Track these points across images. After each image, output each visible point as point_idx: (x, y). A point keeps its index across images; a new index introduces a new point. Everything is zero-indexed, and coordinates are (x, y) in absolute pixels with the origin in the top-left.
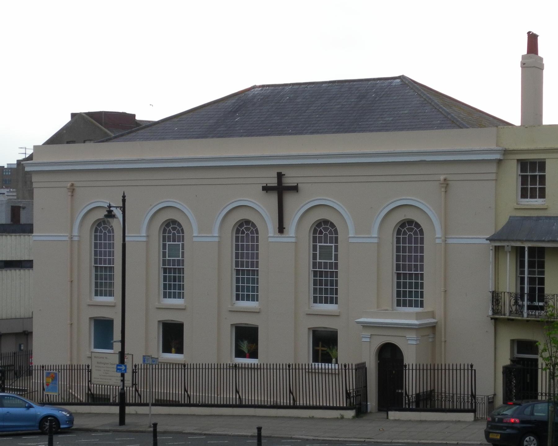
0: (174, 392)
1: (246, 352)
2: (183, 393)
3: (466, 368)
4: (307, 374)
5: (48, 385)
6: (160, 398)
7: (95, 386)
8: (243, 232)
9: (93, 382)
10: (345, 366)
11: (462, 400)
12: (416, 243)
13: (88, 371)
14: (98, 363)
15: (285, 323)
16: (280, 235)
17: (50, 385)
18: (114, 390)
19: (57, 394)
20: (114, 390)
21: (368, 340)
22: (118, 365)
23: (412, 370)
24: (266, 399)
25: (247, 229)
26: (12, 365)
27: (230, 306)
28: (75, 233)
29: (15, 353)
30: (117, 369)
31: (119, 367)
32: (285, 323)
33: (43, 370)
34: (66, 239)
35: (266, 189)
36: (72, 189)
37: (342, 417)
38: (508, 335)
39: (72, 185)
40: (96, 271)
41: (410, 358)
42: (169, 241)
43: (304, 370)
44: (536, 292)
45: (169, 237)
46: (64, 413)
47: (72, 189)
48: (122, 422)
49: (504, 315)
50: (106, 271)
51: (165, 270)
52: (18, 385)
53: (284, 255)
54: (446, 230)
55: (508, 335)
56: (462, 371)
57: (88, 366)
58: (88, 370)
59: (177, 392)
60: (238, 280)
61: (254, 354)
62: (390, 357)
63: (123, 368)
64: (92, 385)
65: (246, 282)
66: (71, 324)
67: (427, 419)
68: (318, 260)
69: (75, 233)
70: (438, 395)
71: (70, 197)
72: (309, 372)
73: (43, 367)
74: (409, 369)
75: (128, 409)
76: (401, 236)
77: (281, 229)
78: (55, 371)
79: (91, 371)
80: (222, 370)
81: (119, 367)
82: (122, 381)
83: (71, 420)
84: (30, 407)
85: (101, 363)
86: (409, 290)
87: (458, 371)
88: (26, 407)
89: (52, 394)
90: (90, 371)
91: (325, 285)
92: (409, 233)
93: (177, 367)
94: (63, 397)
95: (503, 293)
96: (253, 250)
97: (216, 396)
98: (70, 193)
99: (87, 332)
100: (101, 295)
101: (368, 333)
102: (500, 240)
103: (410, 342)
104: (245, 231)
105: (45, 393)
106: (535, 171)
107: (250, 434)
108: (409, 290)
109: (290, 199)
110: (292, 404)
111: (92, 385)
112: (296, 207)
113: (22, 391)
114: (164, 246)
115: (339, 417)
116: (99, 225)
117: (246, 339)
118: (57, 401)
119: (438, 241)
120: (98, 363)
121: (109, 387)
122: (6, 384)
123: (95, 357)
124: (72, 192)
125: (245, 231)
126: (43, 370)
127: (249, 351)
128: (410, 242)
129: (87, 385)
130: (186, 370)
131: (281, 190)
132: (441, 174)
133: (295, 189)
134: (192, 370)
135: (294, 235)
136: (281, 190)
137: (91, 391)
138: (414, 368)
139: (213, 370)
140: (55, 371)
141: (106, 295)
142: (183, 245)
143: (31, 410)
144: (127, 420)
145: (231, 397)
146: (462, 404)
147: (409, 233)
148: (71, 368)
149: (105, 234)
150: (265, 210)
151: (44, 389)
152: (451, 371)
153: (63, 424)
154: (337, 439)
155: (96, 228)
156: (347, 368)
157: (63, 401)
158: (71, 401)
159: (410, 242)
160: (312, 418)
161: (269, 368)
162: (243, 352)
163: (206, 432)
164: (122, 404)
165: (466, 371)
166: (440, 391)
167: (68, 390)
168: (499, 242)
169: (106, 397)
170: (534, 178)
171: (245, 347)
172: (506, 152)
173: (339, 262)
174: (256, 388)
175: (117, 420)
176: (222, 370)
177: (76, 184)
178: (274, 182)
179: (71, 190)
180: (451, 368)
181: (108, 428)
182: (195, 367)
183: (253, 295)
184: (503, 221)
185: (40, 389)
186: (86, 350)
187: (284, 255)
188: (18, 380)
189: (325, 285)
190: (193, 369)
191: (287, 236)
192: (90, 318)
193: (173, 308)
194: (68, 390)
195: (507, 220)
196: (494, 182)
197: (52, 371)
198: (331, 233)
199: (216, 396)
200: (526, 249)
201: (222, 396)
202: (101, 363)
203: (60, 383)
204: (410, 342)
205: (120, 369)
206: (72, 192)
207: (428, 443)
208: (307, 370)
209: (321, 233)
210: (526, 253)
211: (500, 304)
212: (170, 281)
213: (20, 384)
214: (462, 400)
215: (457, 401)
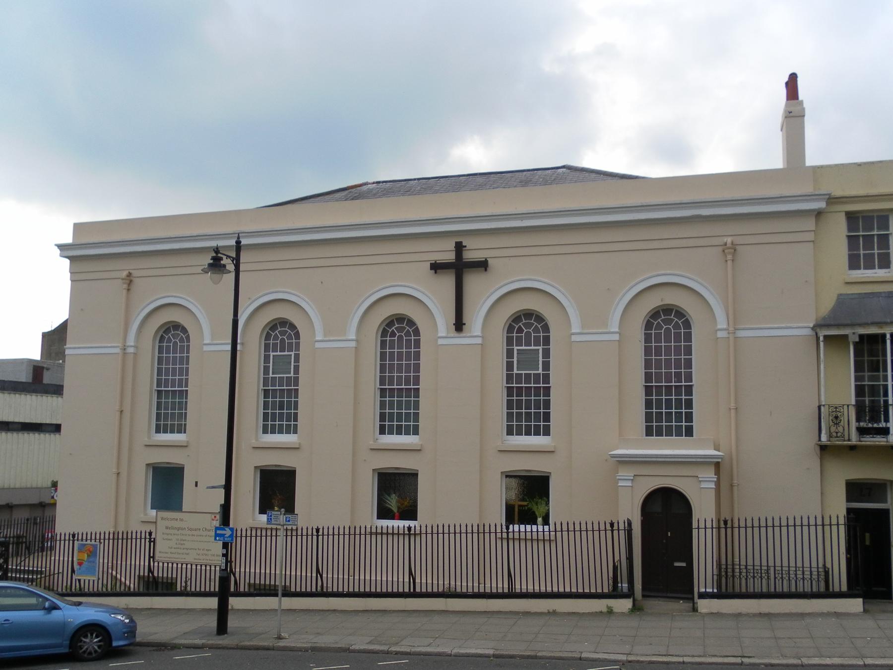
0: (263, 571)
1: (395, 510)
2: (407, 580)
3: (602, 527)
4: (499, 542)
5: (80, 564)
6: (257, 582)
7: (161, 564)
8: (393, 334)
9: (157, 558)
10: (318, 530)
11: (792, 576)
12: (408, 346)
13: (150, 542)
14: (167, 528)
15: (462, 465)
16: (457, 335)
17: (85, 565)
18: (203, 572)
19: (96, 579)
20: (203, 572)
21: (629, 484)
22: (217, 529)
23: (360, 534)
24: (430, 581)
25: (400, 330)
26: (23, 536)
27: (371, 442)
28: (131, 341)
29: (28, 520)
30: (216, 535)
31: (218, 532)
32: (462, 465)
33: (73, 541)
34: (117, 350)
35: (436, 267)
36: (129, 280)
37: (610, 612)
38: (843, 473)
39: (130, 275)
40: (159, 397)
41: (704, 511)
42: (275, 350)
43: (493, 535)
44: (871, 409)
45: (275, 345)
46: (119, 617)
47: (129, 280)
48: (222, 628)
49: (849, 440)
50: (174, 397)
51: (266, 393)
52: (31, 564)
53: (462, 368)
54: (735, 319)
55: (843, 473)
56: (458, 536)
57: (150, 534)
58: (150, 539)
59: (304, 574)
60: (382, 405)
61: (410, 513)
62: (666, 512)
63: (228, 532)
64: (156, 564)
65: (398, 406)
66: (118, 474)
67: (772, 612)
68: (515, 371)
69: (131, 341)
70: (727, 568)
71: (125, 292)
72: (508, 539)
73: (74, 536)
74: (323, 535)
75: (234, 602)
76: (653, 332)
77: (459, 325)
78: (93, 542)
79: (154, 542)
80: (357, 537)
81: (218, 532)
82: (223, 555)
83: (131, 630)
84: (56, 607)
85: (173, 528)
86: (668, 406)
87: (763, 530)
88: (44, 609)
89: (87, 578)
90: (152, 541)
91: (528, 405)
92: (667, 328)
93: (259, 534)
94: (105, 582)
95: (846, 407)
96: (289, 408)
97: (346, 577)
98: (125, 286)
99: (141, 485)
100: (165, 432)
101: (626, 473)
102: (838, 326)
103: (703, 485)
104: (399, 334)
105: (74, 577)
106: (872, 229)
107: (491, 652)
108: (668, 406)
109: (473, 282)
110: (506, 591)
111: (156, 564)
112: (482, 294)
113: (32, 577)
114: (267, 358)
115: (605, 610)
116: (167, 331)
117: (397, 492)
118: (96, 589)
119: (720, 334)
120: (167, 528)
121: (184, 566)
122: (10, 563)
123: (162, 519)
124: (129, 285)
125: (399, 334)
126: (73, 541)
127: (399, 508)
128: (668, 340)
129: (147, 564)
130: (321, 537)
131: (460, 267)
132: (727, 234)
133: (483, 265)
134: (331, 537)
135: (479, 334)
136: (460, 267)
137: (153, 573)
138: (347, 532)
139: (441, 536)
140: (93, 542)
141: (172, 432)
142: (297, 357)
143: (55, 613)
144: (232, 622)
145: (502, 586)
146: (793, 582)
147: (667, 328)
148: (115, 537)
149: (400, 337)
150: (434, 299)
151: (73, 571)
152: (464, 535)
153: (120, 639)
154: (681, 659)
155: (162, 336)
156: (321, 533)
157: (104, 590)
158: (118, 589)
159: (668, 340)
160: (554, 613)
161: (435, 532)
162: (390, 511)
163: (397, 649)
164: (224, 593)
165: (603, 533)
166: (743, 563)
167: (110, 571)
168: (830, 335)
169: (165, 581)
170: (868, 239)
171: (393, 502)
172: (832, 200)
173: (552, 373)
174: (579, 566)
175: (212, 622)
176: (357, 537)
177: (135, 273)
178: (450, 257)
179: (128, 282)
180: (463, 530)
181: (198, 642)
182: (441, 531)
183: (408, 427)
184: (828, 304)
185: (67, 571)
186: (141, 512)
187: (462, 368)
188: (31, 557)
189: (528, 405)
190: (109, 539)
191: (469, 335)
192: (148, 465)
193: (398, 450)
194: (110, 571)
195: (835, 299)
196: (811, 244)
197: (89, 542)
198: (536, 330)
199: (346, 577)
200: (888, 336)
201: (357, 577)
202: (173, 528)
203: (101, 561)
204: (703, 485)
205: (220, 535)
206: (129, 285)
207: (877, 666)
208: (499, 535)
209: (520, 330)
210: (888, 342)
211: (842, 423)
212: (274, 408)
213: (33, 562)
214: (792, 576)
215: (775, 578)
